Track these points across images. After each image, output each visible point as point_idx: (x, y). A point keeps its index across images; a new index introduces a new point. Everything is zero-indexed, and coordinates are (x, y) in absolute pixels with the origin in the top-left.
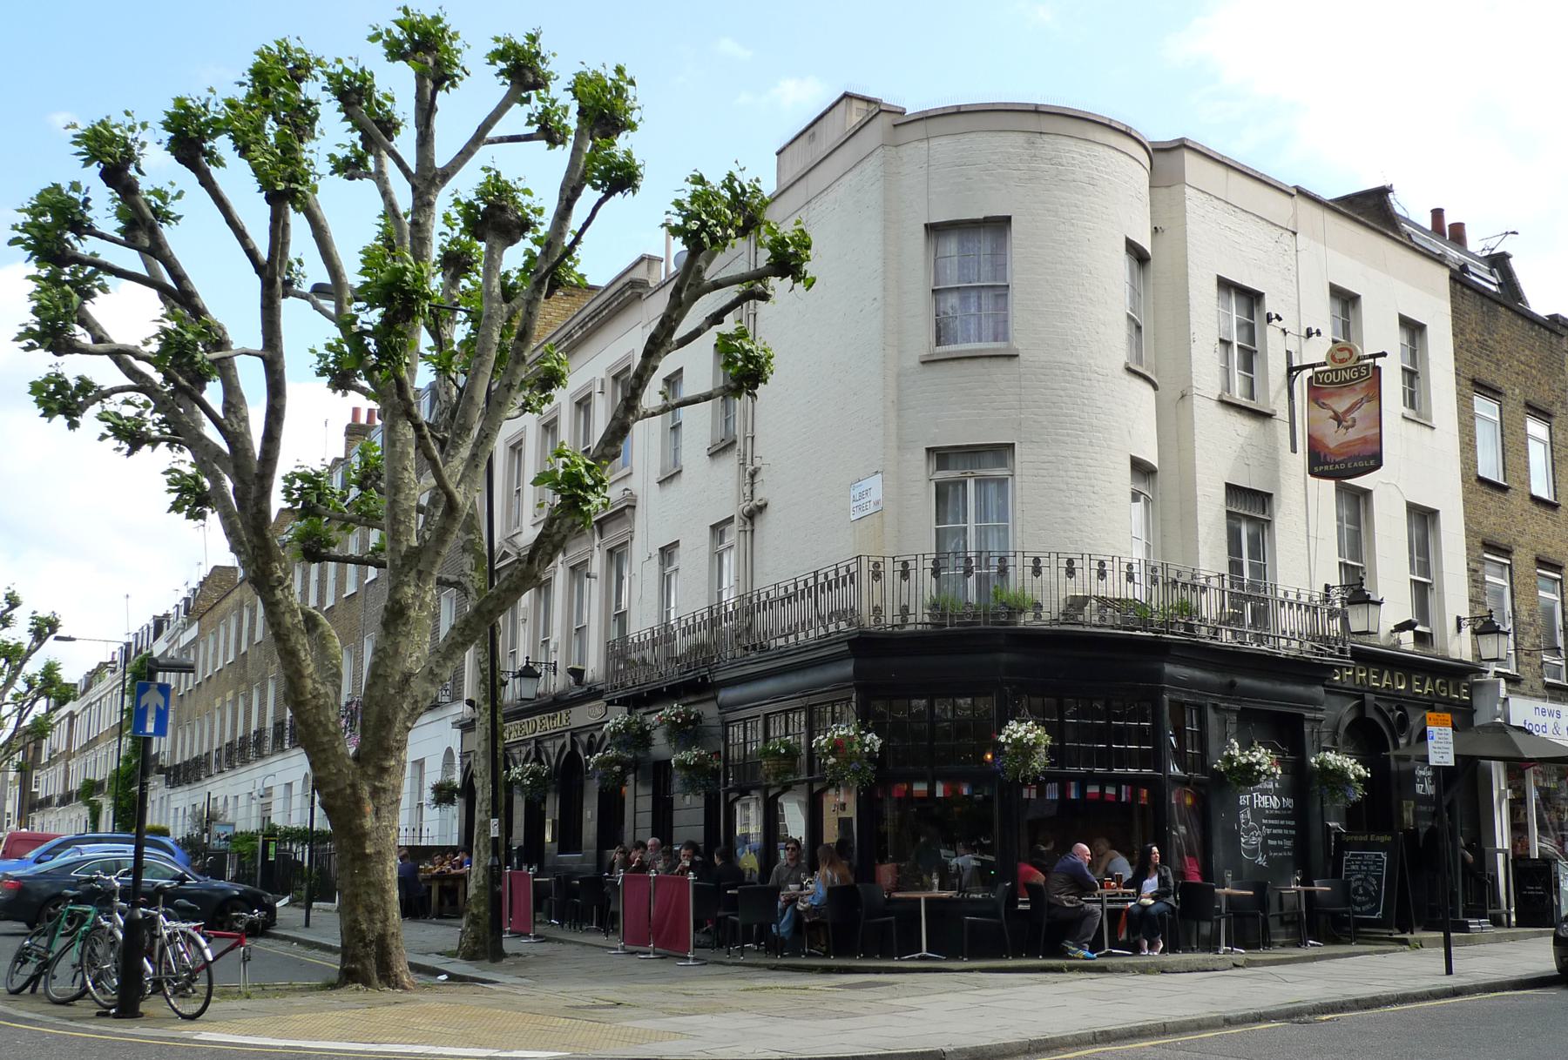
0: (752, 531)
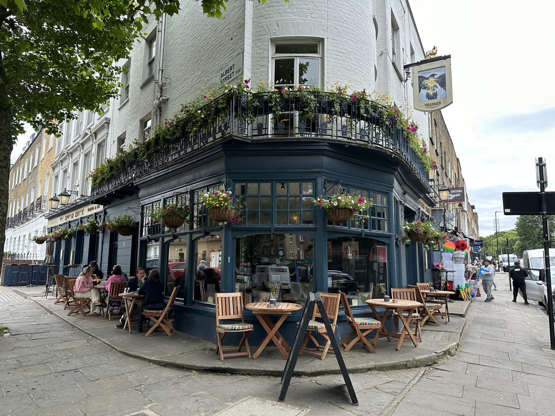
0: (160, 115)
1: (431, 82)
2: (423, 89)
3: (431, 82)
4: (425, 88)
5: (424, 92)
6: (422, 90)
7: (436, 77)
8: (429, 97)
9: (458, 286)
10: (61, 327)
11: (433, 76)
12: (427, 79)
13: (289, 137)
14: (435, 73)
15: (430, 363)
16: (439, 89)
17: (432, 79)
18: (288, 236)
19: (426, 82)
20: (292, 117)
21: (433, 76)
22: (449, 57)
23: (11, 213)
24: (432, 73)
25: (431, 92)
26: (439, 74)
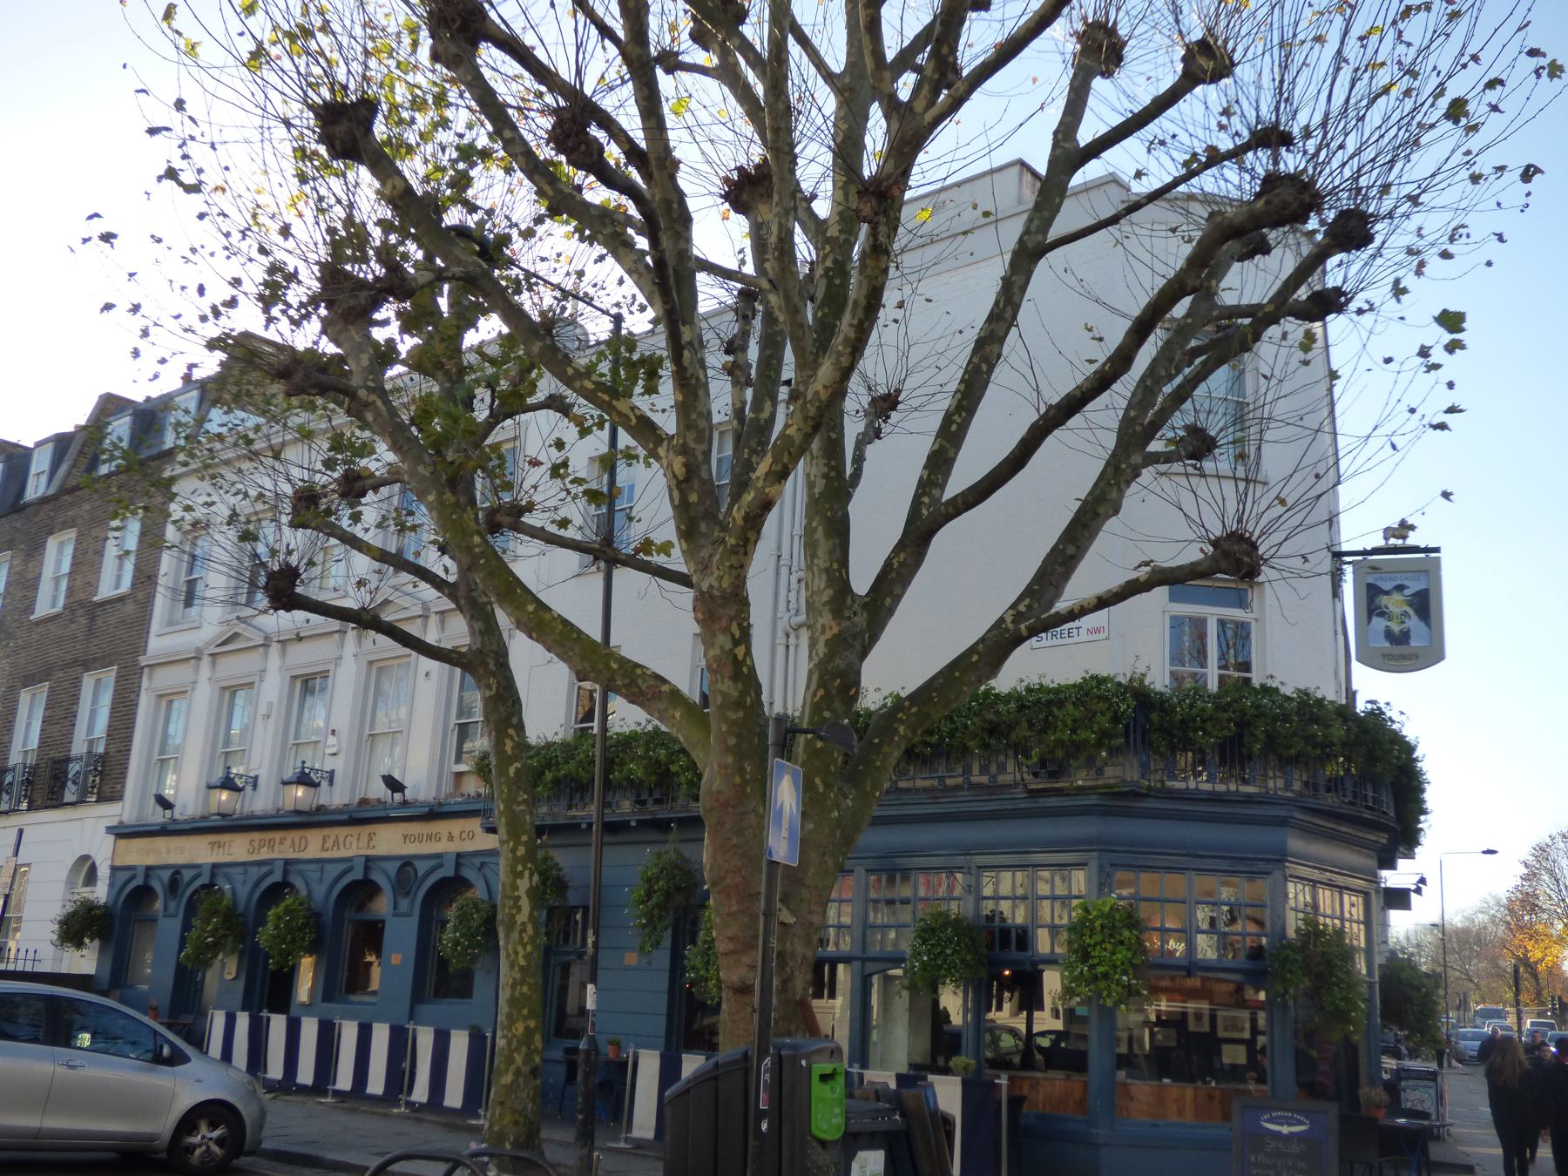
1: (1395, 603)
2: (1377, 615)
3: (1395, 603)
4: (1382, 614)
5: (1379, 623)
6: (1375, 620)
7: (1407, 592)
8: (1389, 635)
9: (1495, 897)
10: (266, 727)
11: (1400, 588)
12: (1387, 593)
13: (597, 753)
14: (1406, 583)
15: (68, 498)
16: (1414, 623)
17: (1396, 597)
18: (841, 967)
19: (1384, 600)
20: (1225, 1018)
21: (1400, 588)
22: (1437, 550)
23: (596, 634)
24: (1399, 582)
25: (1396, 628)
26: (1414, 587)
